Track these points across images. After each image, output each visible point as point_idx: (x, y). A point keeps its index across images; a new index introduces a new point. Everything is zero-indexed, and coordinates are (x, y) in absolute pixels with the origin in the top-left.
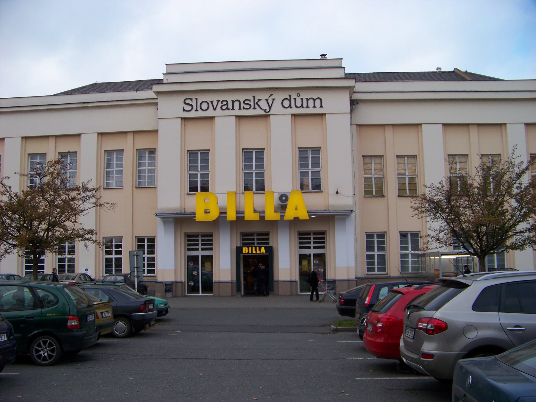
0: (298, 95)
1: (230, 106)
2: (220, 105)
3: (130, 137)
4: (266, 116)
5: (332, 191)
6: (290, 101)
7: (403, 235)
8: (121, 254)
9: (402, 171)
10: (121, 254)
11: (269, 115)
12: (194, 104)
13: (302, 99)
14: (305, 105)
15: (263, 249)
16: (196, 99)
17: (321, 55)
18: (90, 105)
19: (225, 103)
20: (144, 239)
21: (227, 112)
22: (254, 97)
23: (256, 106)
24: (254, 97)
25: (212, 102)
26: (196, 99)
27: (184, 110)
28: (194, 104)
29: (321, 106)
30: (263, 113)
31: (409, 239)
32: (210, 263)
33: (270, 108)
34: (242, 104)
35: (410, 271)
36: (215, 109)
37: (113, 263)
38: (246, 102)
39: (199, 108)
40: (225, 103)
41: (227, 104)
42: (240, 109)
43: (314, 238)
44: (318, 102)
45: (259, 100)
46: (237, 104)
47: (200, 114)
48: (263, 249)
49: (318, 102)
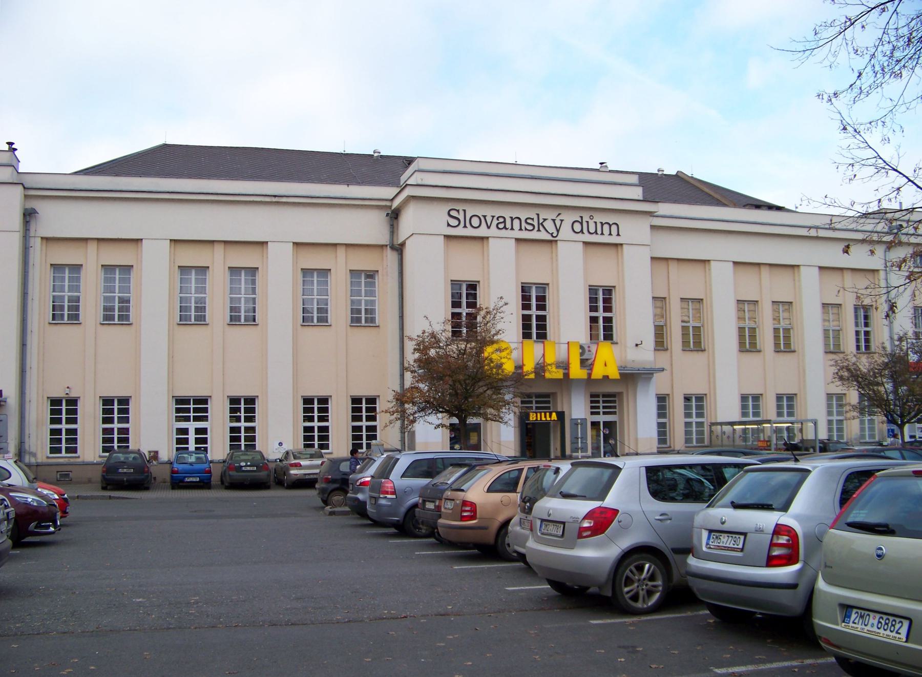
0: (591, 217)
1: (508, 225)
2: (495, 222)
3: (341, 252)
4: (552, 242)
5: (631, 343)
6: (581, 223)
7: (687, 399)
8: (51, 430)
9: (686, 319)
10: (51, 430)
11: (556, 241)
12: (461, 217)
13: (596, 223)
14: (599, 231)
15: (554, 415)
16: (465, 211)
17: (601, 163)
18: (284, 200)
19: (501, 220)
20: (240, 400)
21: (504, 233)
22: (538, 215)
23: (541, 228)
24: (538, 215)
25: (485, 217)
26: (465, 211)
27: (449, 225)
28: (461, 217)
29: (618, 235)
30: (549, 237)
31: (694, 403)
32: (476, 434)
33: (558, 231)
34: (524, 224)
35: (695, 443)
36: (489, 227)
37: (316, 434)
38: (529, 221)
39: (468, 224)
40: (501, 220)
41: (504, 222)
42: (521, 229)
43: (604, 402)
44: (614, 228)
45: (545, 220)
46: (516, 223)
47: (470, 232)
48: (554, 415)
49: (614, 228)
